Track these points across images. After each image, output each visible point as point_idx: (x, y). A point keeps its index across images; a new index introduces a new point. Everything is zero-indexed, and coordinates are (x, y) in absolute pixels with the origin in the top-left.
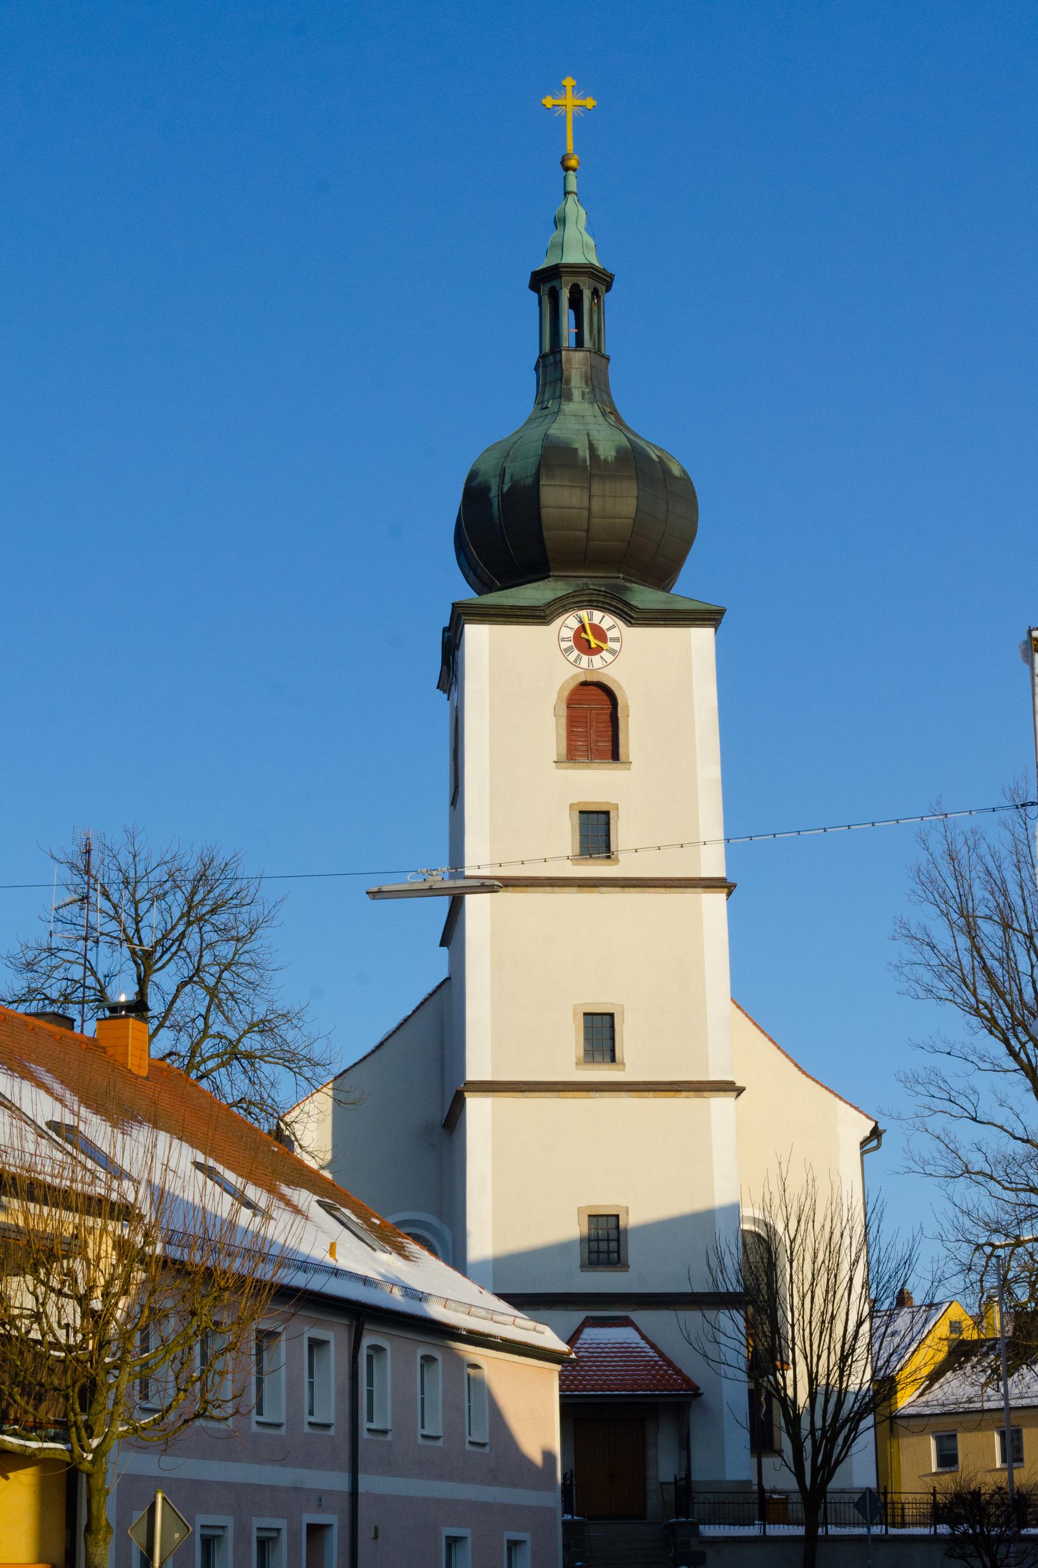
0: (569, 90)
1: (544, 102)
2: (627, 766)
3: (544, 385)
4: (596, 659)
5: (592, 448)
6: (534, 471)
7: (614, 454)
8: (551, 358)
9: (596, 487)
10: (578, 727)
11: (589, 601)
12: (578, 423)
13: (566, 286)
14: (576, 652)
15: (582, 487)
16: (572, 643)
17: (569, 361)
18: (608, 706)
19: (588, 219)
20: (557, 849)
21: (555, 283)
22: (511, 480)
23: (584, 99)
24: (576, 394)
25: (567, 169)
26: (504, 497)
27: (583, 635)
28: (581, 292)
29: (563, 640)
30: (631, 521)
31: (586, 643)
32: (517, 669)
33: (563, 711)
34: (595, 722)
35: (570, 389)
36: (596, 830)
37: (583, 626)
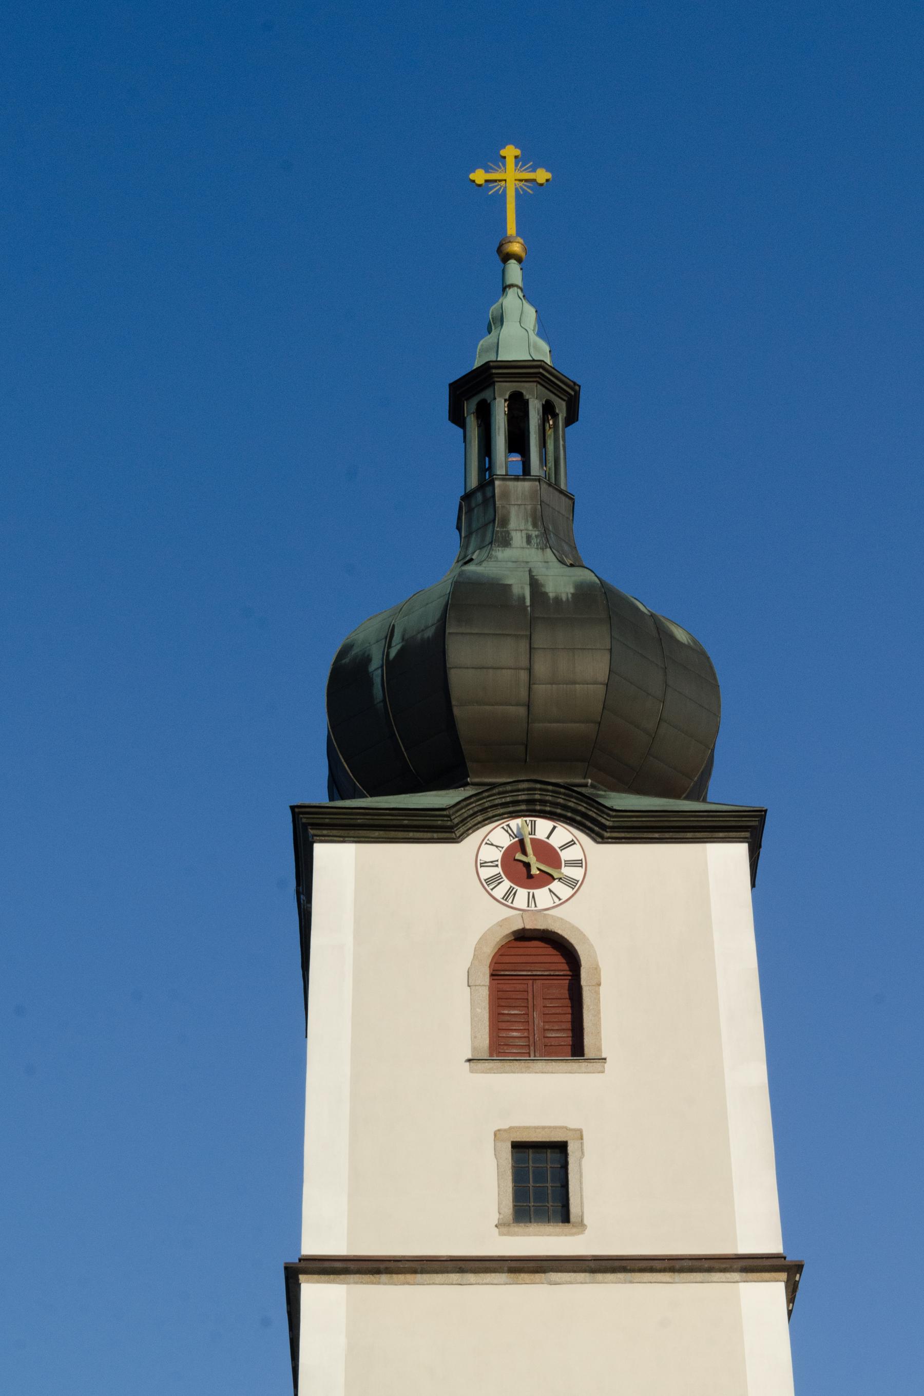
0: (510, 162)
1: (472, 176)
2: (598, 1065)
3: (468, 536)
4: (543, 896)
5: (535, 584)
6: (438, 615)
7: (571, 590)
8: (479, 496)
9: (541, 638)
10: (514, 1007)
11: (528, 802)
12: (519, 561)
13: (500, 396)
14: (506, 884)
15: (516, 636)
16: (499, 870)
17: (506, 495)
18: (562, 967)
19: (539, 319)
20: (475, 1211)
21: (486, 395)
22: (403, 639)
23: (534, 171)
24: (518, 538)
25: (506, 257)
26: (390, 666)
27: (519, 856)
28: (526, 403)
30: (601, 689)
31: (527, 867)
33: (484, 978)
34: (539, 995)
35: (508, 533)
36: (541, 1175)
37: (522, 842)
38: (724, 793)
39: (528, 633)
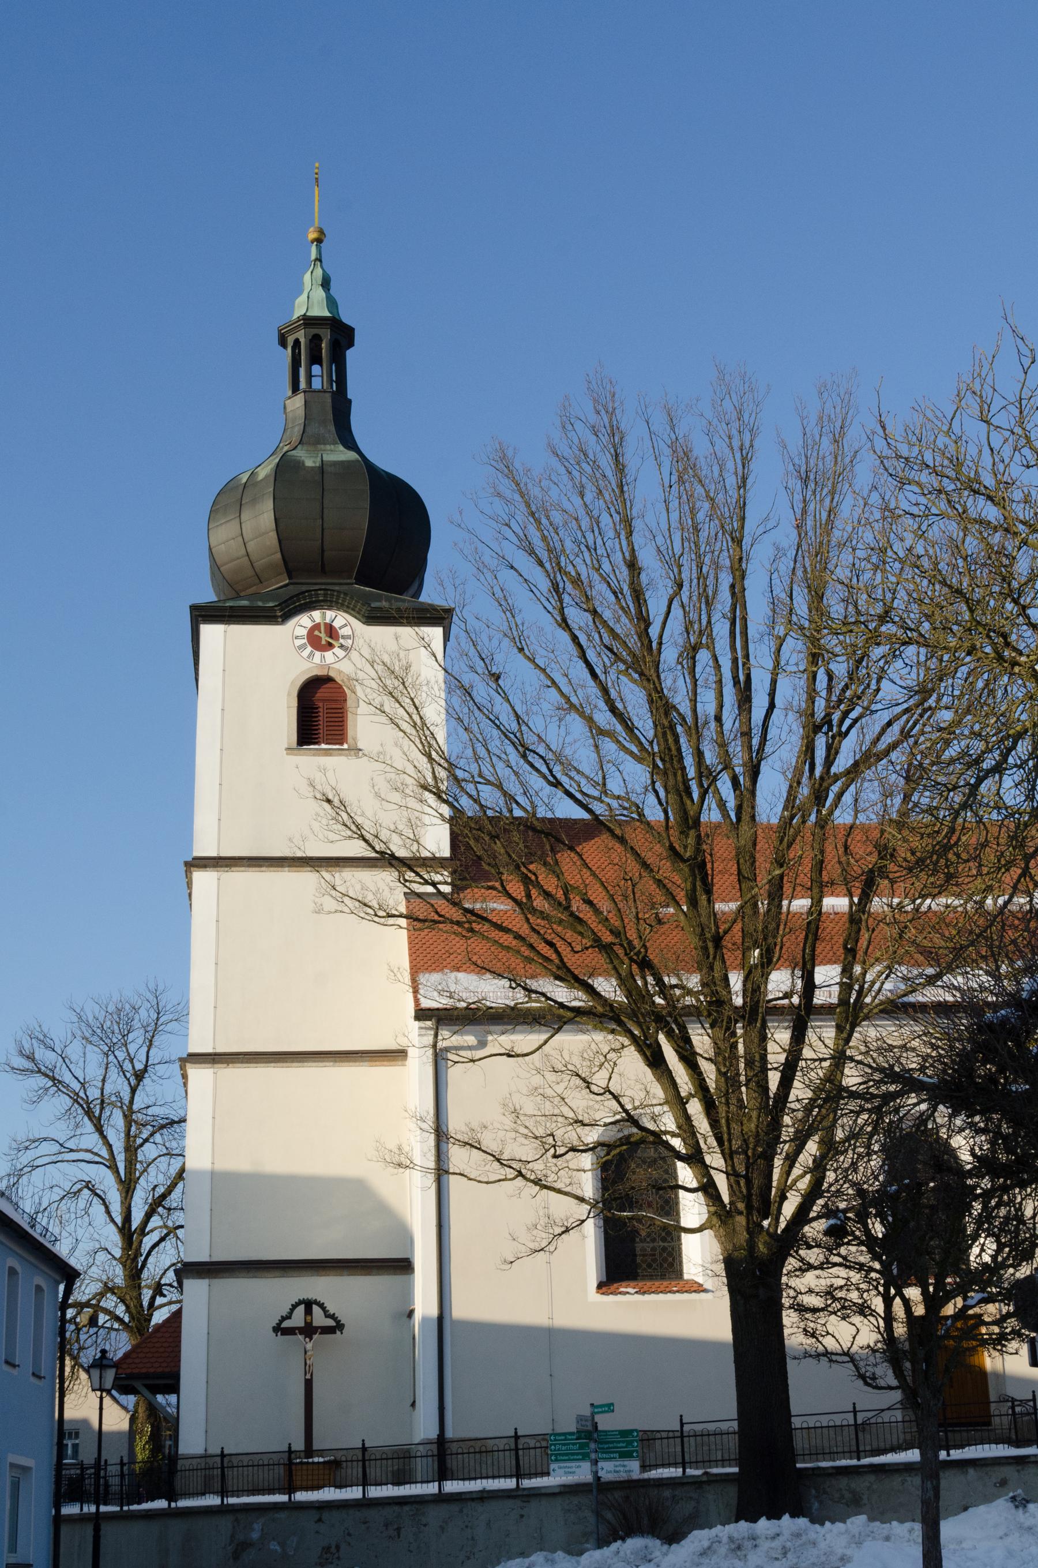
4: (329, 656)
14: (309, 649)
16: (305, 641)
27: (316, 633)
29: (296, 638)
31: (323, 639)
32: (254, 667)
34: (318, 714)
38: (430, 594)
39: (222, 569)
